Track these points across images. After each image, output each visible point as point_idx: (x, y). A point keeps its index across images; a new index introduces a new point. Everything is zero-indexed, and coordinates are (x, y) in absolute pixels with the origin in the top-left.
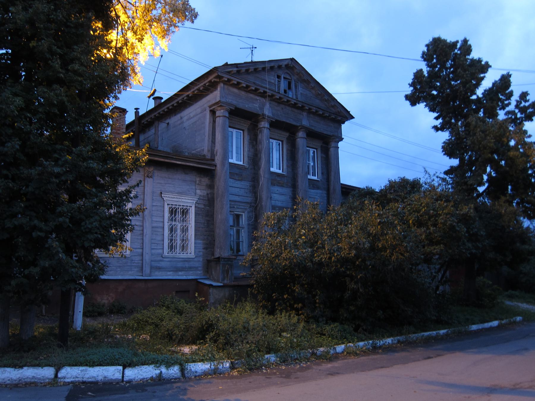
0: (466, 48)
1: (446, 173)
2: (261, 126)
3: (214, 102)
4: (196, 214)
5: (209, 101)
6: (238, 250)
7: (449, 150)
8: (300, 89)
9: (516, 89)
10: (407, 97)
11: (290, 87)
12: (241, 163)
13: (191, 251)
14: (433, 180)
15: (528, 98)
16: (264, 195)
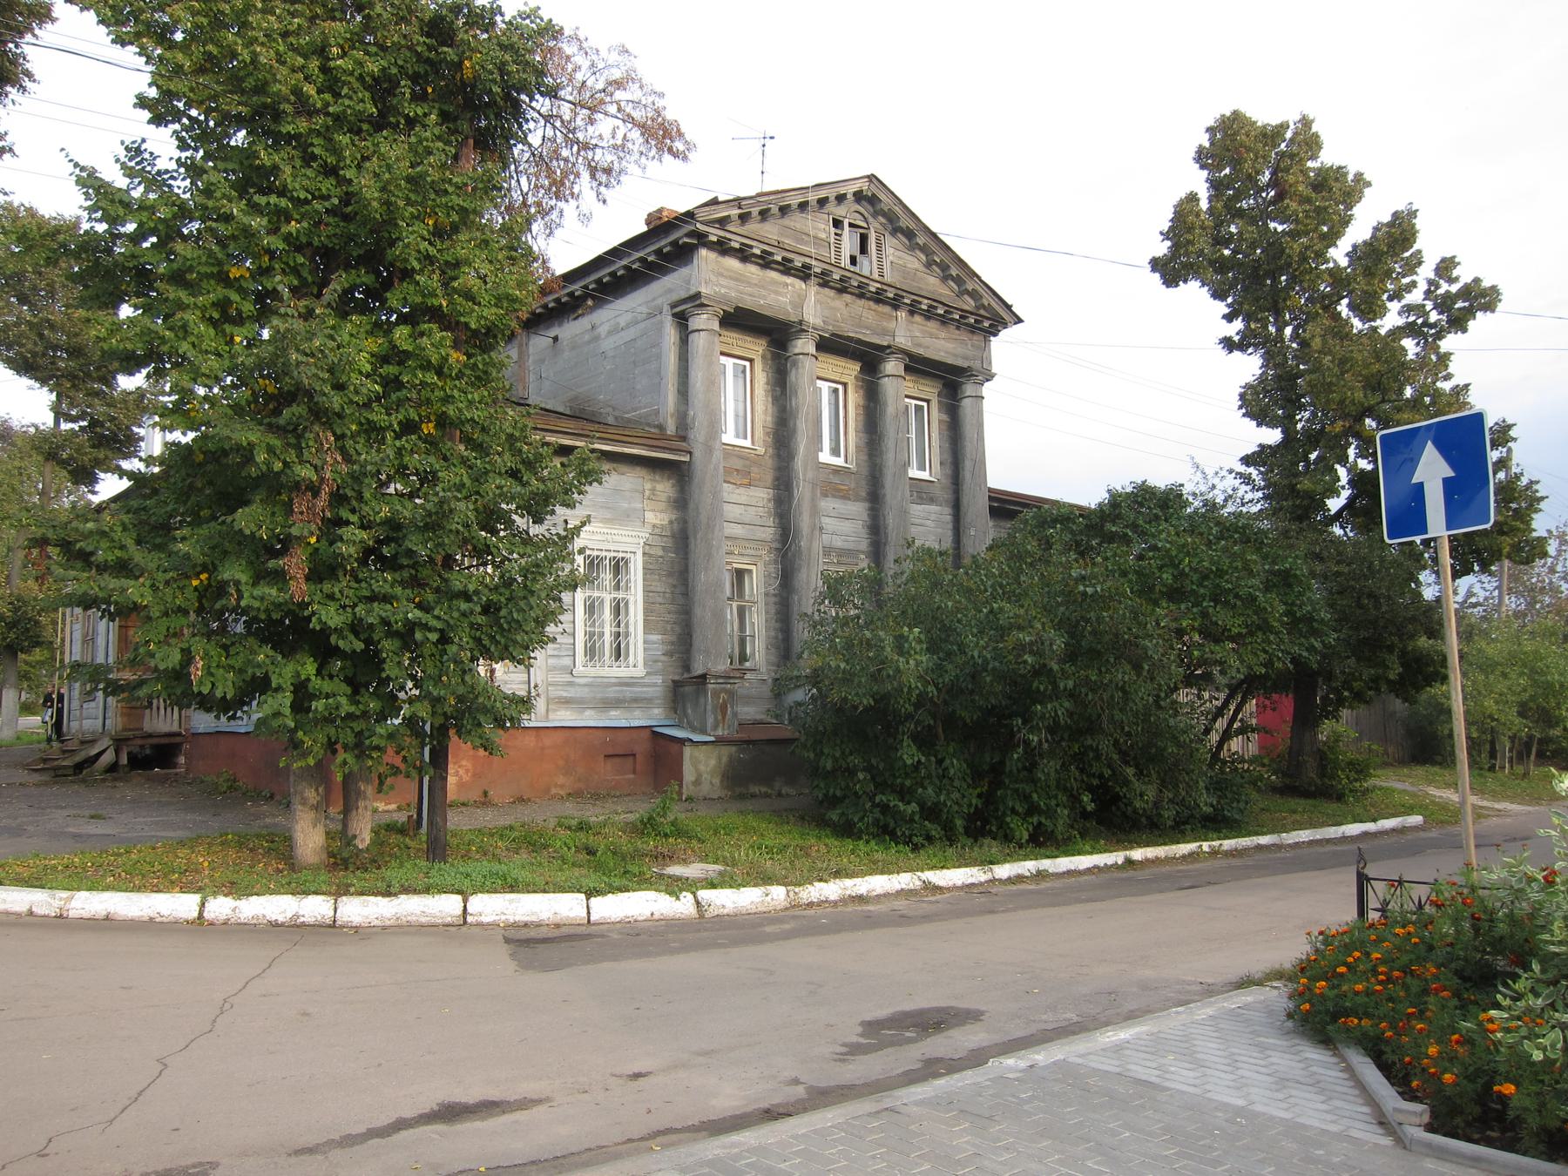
0: (1308, 141)
1: (1247, 460)
2: (797, 351)
3: (684, 295)
4: (647, 570)
5: (670, 291)
6: (743, 658)
7: (1256, 404)
8: (890, 251)
9: (1430, 245)
10: (1156, 264)
11: (864, 249)
12: (747, 443)
13: (636, 665)
14: (1214, 487)
15: (1455, 273)
16: (804, 522)
